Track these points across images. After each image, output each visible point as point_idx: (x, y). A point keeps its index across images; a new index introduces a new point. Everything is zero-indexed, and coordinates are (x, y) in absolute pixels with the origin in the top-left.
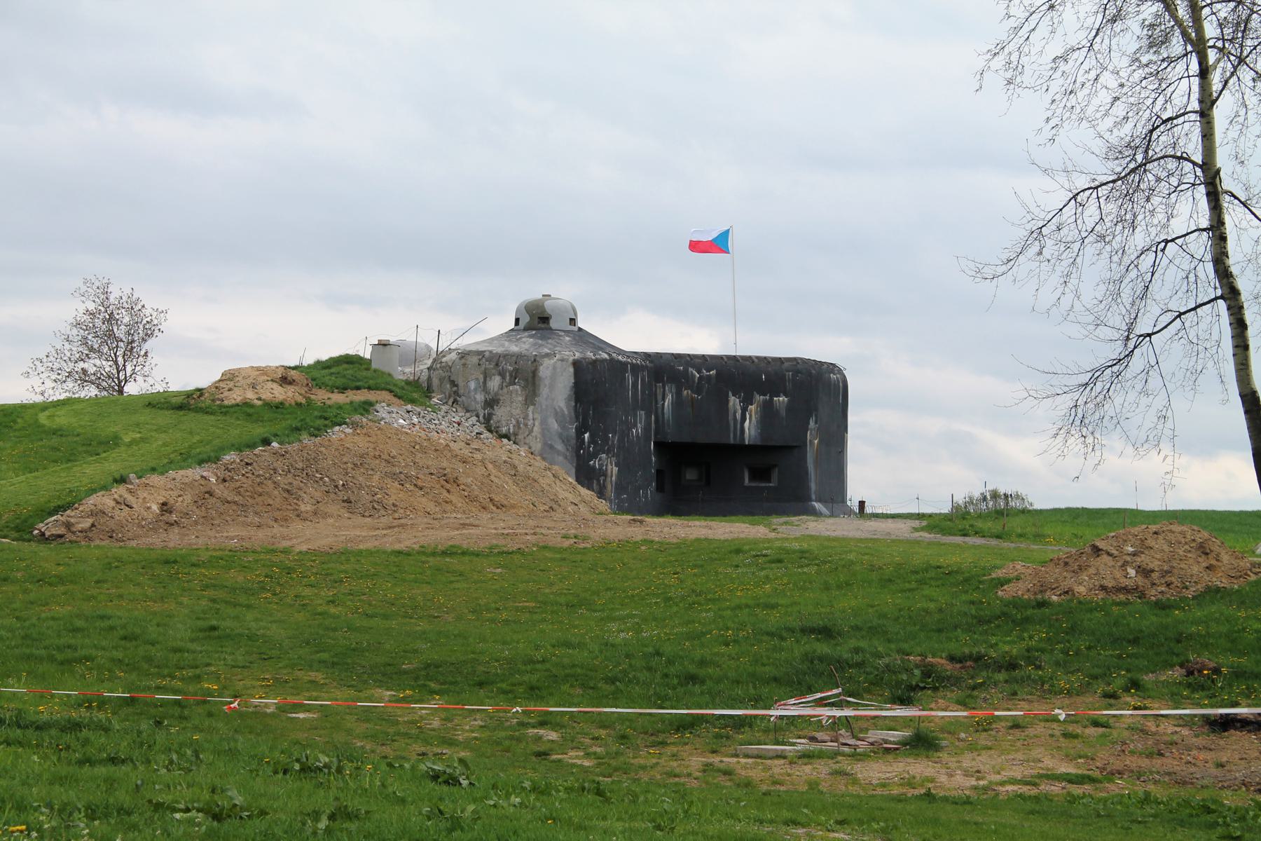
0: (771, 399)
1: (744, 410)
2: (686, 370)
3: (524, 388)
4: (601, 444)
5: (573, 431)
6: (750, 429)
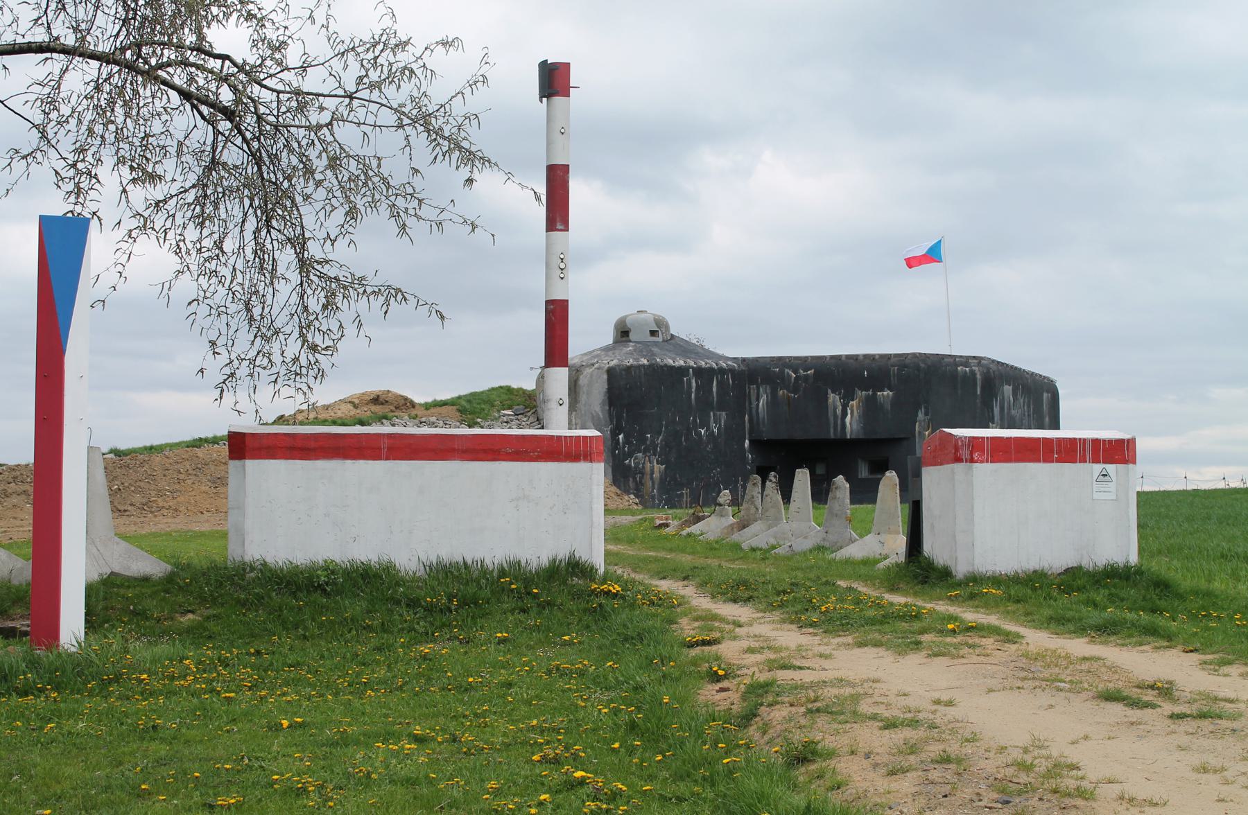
0: (875, 394)
1: (845, 407)
2: (782, 372)
6: (852, 423)
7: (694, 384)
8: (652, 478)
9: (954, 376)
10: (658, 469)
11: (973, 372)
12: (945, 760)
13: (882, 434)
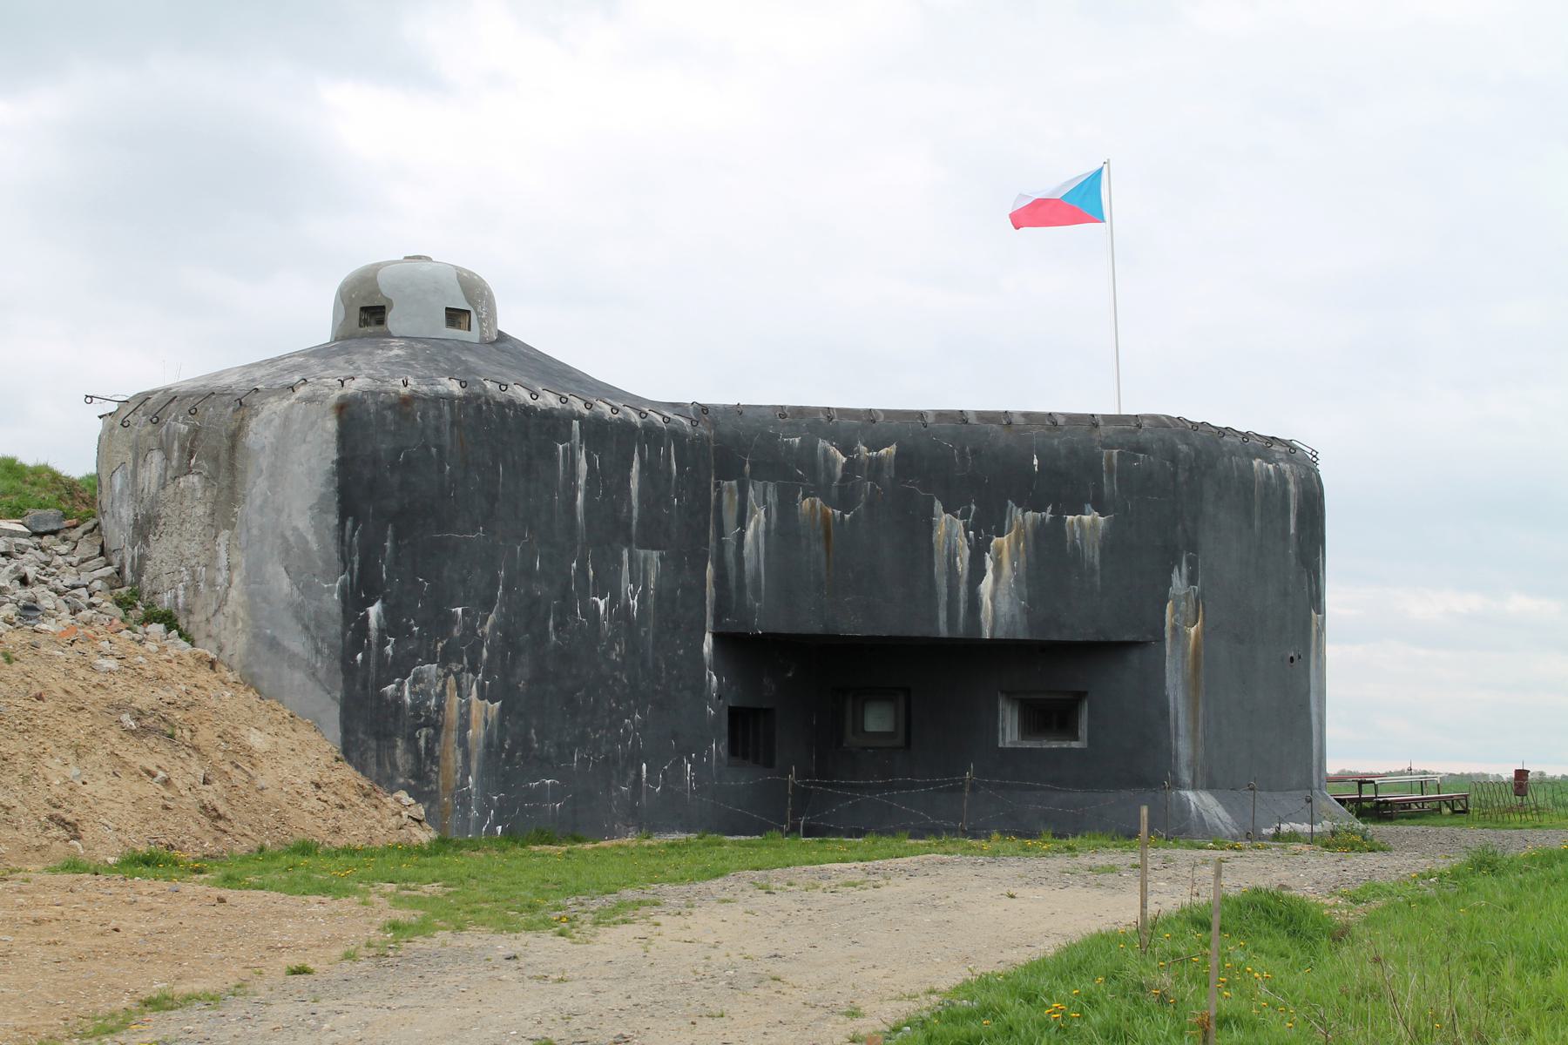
0: (1058, 520)
1: (978, 552)
3: (210, 480)
4: (426, 631)
5: (332, 601)
6: (998, 601)
7: (583, 466)
8: (463, 742)
9: (1246, 480)
10: (483, 712)
11: (1280, 474)
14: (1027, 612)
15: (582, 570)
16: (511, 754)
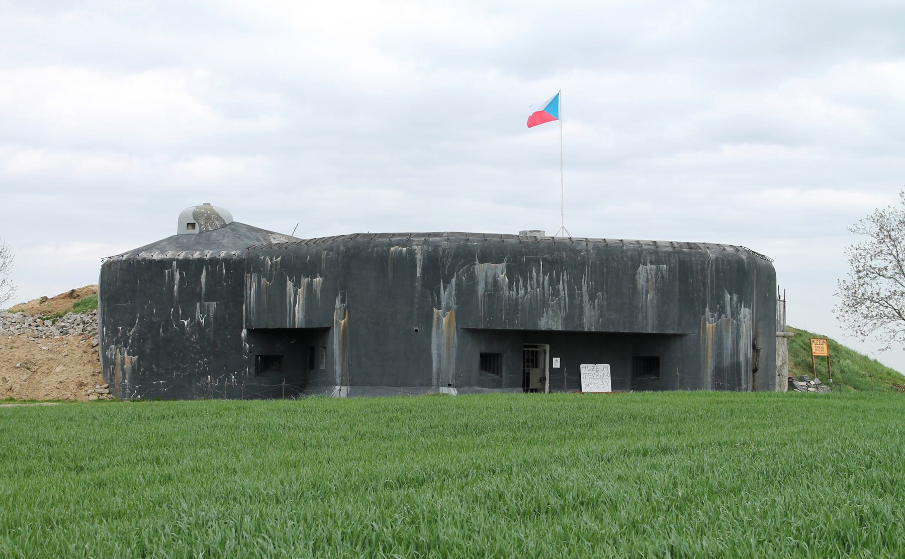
0: (312, 280)
7: (177, 276)
8: (122, 369)
10: (129, 360)
12: (894, 513)
13: (316, 325)
14: (305, 317)
15: (176, 311)
16: (144, 373)
